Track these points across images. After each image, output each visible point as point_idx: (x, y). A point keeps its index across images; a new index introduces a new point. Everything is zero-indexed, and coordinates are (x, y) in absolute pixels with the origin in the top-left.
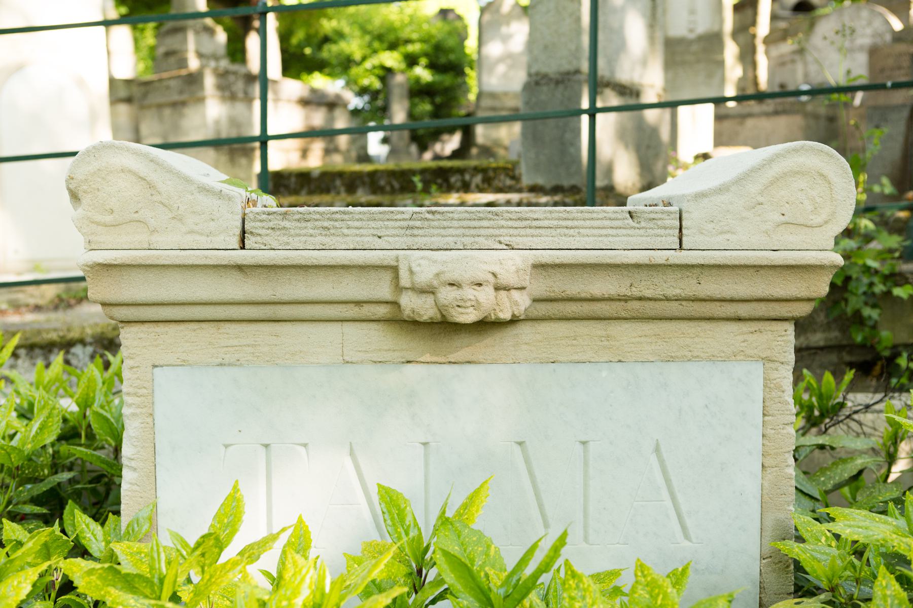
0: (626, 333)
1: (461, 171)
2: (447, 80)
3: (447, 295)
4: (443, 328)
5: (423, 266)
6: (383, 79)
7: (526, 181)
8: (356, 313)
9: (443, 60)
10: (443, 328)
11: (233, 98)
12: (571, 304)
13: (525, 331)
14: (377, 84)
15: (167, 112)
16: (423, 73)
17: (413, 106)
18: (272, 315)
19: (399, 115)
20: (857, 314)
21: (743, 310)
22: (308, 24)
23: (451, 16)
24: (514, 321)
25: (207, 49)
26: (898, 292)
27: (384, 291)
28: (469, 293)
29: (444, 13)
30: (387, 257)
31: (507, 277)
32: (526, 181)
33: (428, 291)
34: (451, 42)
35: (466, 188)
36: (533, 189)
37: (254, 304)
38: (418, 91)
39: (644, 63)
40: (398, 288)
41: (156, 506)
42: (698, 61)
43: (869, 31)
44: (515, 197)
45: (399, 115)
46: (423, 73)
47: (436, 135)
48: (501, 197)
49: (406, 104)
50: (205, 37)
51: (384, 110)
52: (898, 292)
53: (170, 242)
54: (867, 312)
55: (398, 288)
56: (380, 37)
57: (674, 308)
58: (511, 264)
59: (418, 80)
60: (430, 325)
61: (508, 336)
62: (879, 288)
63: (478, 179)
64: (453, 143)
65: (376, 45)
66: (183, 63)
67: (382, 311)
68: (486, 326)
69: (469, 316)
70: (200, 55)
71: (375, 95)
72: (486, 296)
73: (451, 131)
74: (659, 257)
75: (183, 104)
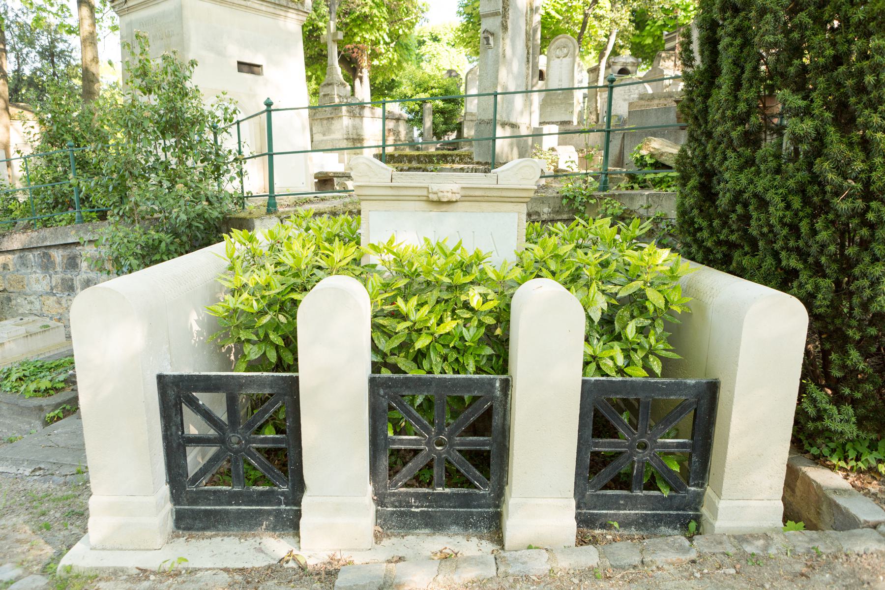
0: (484, 205)
1: (451, 156)
2: (451, 106)
3: (440, 194)
4: (439, 202)
5: (435, 187)
6: (420, 106)
7: (475, 160)
8: (419, 198)
9: (449, 97)
10: (439, 202)
11: (354, 116)
12: (470, 197)
13: (459, 203)
14: (417, 108)
15: (325, 122)
16: (440, 104)
17: (434, 118)
18: (398, 199)
19: (428, 122)
20: (577, 208)
21: (513, 200)
22: (384, 74)
23: (453, 74)
24: (456, 201)
25: (342, 93)
26: (591, 201)
27: (425, 193)
28: (446, 194)
29: (450, 72)
30: (426, 185)
31: (454, 191)
32: (475, 160)
33: (436, 193)
34: (453, 88)
35: (453, 162)
36: (478, 163)
37: (395, 196)
38: (437, 111)
39: (522, 113)
40: (429, 193)
41: (290, 341)
42: (562, 103)
43: (637, 91)
44: (471, 166)
45: (428, 122)
46: (440, 104)
47: (445, 132)
48: (466, 166)
49: (431, 117)
50: (342, 88)
51: (421, 121)
52: (591, 201)
53: (374, 181)
54: (580, 208)
55: (429, 193)
56: (420, 85)
57: (496, 199)
58: (456, 187)
59: (437, 107)
60: (436, 202)
61: (455, 205)
62: (585, 200)
63: (458, 159)
64: (452, 136)
65: (418, 89)
66: (332, 99)
67: (425, 198)
68: (449, 202)
69: (445, 200)
70: (340, 96)
71: (417, 113)
72: (449, 195)
73: (452, 131)
74: (492, 186)
75: (332, 118)
